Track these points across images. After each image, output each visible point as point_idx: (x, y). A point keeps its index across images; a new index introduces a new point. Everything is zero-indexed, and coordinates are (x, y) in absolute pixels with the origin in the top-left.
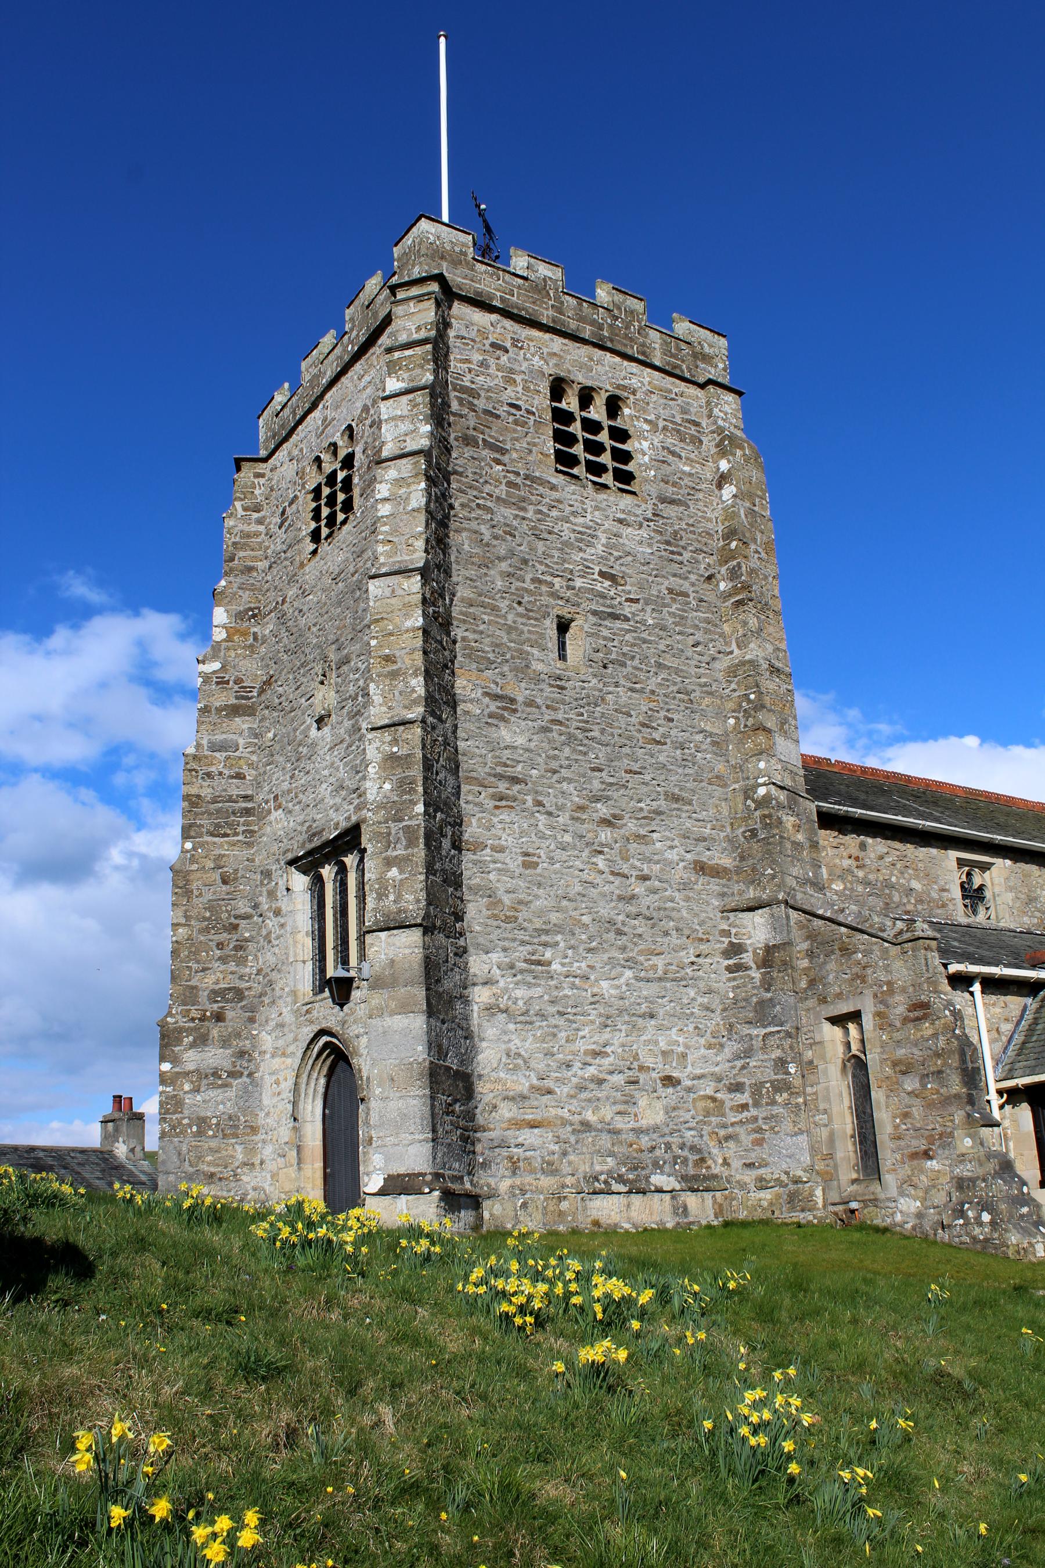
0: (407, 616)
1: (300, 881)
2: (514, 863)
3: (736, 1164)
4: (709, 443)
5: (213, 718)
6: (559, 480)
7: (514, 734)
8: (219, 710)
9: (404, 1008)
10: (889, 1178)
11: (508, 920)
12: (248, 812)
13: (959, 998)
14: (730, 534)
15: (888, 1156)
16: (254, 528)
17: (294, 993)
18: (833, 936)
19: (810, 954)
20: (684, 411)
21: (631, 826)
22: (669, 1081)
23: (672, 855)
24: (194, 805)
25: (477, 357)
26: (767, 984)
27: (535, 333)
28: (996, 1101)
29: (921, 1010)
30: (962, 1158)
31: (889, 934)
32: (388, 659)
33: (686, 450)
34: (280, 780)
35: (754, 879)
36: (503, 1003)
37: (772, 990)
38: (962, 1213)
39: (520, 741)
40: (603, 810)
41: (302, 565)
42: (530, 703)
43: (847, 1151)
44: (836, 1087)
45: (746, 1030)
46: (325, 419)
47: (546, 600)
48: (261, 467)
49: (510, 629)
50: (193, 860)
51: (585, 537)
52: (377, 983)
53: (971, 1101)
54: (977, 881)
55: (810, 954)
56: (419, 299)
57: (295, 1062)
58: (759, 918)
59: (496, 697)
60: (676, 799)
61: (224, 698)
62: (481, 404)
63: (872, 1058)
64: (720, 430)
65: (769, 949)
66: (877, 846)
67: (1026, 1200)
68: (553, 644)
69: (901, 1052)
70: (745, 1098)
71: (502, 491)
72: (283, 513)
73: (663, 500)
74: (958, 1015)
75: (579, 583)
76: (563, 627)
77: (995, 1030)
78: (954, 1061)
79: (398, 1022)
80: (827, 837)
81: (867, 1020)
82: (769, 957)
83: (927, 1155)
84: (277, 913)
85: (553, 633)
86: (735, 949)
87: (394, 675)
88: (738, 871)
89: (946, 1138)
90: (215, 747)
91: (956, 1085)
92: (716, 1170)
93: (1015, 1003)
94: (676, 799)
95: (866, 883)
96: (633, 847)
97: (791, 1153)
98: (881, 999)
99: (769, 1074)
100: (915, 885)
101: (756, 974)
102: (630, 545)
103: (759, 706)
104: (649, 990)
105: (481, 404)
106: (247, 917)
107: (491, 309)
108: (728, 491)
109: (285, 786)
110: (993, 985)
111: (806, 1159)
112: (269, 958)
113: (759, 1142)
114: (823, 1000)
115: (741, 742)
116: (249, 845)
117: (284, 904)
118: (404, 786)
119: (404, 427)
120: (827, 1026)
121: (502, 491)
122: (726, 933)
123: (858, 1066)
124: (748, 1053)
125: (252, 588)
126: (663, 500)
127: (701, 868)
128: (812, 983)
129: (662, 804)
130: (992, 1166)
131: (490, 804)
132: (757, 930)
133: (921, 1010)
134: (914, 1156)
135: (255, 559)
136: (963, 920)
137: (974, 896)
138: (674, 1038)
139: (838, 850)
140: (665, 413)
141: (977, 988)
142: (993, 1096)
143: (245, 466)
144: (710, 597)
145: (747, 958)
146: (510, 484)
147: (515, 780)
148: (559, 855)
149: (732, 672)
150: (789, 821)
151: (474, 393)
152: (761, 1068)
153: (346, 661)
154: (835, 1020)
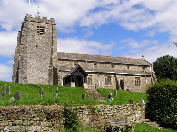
2: (31, 64)
7: (32, 55)
13: (60, 73)
40: (39, 60)
96: (41, 62)
102: (43, 39)
127: (47, 63)
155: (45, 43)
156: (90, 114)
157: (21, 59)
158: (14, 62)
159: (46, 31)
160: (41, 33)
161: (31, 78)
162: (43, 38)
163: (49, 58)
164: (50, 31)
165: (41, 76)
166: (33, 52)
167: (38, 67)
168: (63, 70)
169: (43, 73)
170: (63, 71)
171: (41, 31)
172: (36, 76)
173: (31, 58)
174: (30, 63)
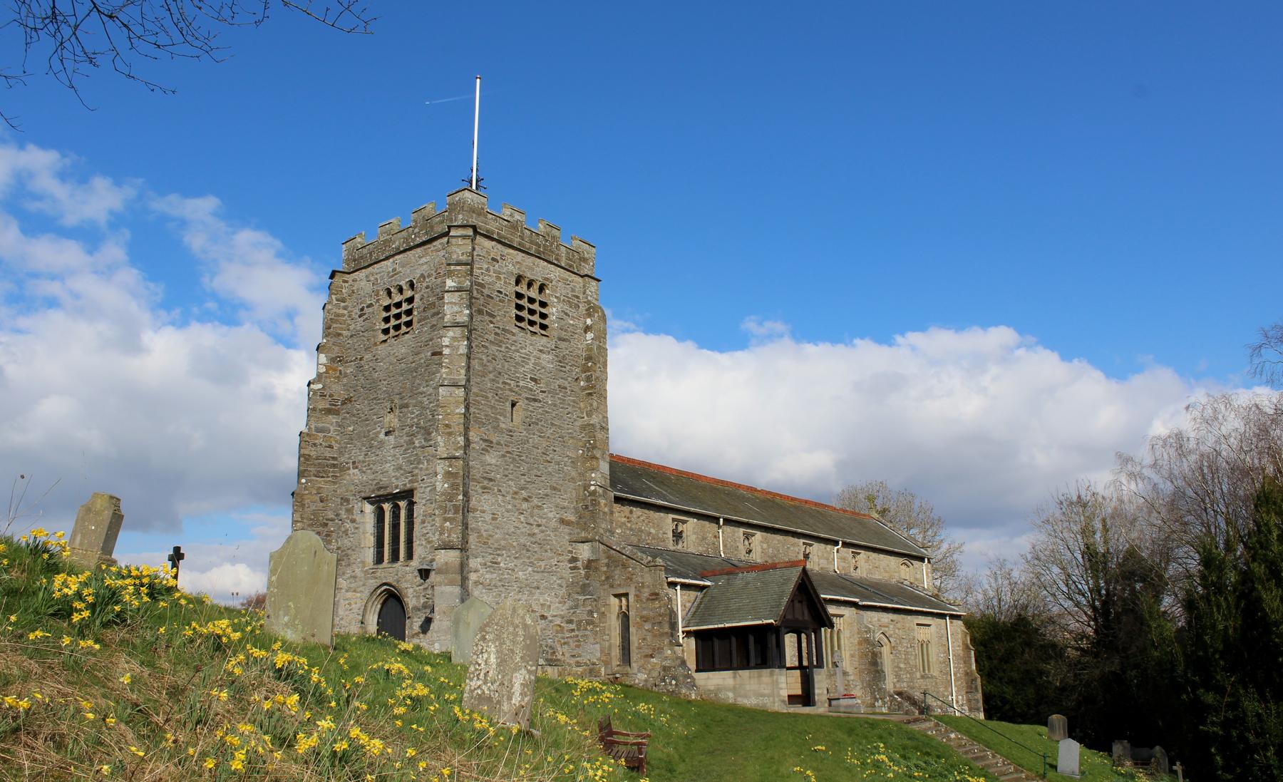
0: (457, 407)
1: (369, 508)
2: (488, 517)
3: (567, 655)
4: (583, 308)
5: (318, 414)
6: (516, 330)
7: (491, 458)
8: (321, 410)
9: (451, 583)
10: (634, 665)
11: (485, 543)
12: (334, 466)
13: (671, 591)
14: (589, 358)
15: (635, 656)
16: (341, 311)
17: (363, 562)
18: (616, 559)
19: (608, 565)
20: (573, 290)
21: (535, 501)
22: (543, 617)
23: (551, 515)
24: (307, 460)
25: (485, 266)
26: (587, 577)
27: (511, 251)
28: (681, 635)
29: (655, 596)
30: (666, 658)
31: (645, 562)
32: (447, 426)
33: (572, 312)
34: (356, 453)
35: (585, 528)
36: (481, 580)
37: (589, 580)
38: (664, 681)
39: (494, 461)
40: (524, 494)
41: (375, 344)
42: (499, 444)
43: (616, 652)
44: (614, 624)
45: (576, 596)
46: (394, 270)
47: (508, 392)
48: (347, 277)
49: (492, 407)
50: (306, 488)
51: (525, 360)
52: (439, 572)
53: (672, 635)
54: (680, 529)
55: (608, 565)
56: (464, 237)
57: (367, 593)
58: (586, 546)
59: (485, 441)
60: (555, 489)
61: (323, 405)
62: (486, 291)
63: (632, 614)
64: (589, 302)
65: (590, 561)
66: (637, 511)
67: (689, 676)
68: (509, 415)
69: (645, 613)
70: (573, 626)
71: (492, 337)
72: (362, 309)
73: (560, 339)
74: (670, 599)
75: (521, 384)
76: (513, 405)
77: (684, 606)
78: (667, 619)
79: (448, 589)
80: (617, 507)
81: (631, 598)
82: (589, 565)
83: (652, 656)
84: (353, 521)
85: (509, 409)
86: (574, 560)
87: (450, 434)
88: (578, 523)
89: (660, 650)
90: (319, 430)
91: (667, 629)
92: (559, 657)
93: (693, 594)
94: (555, 489)
95: (631, 529)
96: (536, 511)
97: (592, 652)
98: (639, 589)
99: (585, 617)
100: (653, 531)
101: (583, 572)
102: (544, 363)
103: (594, 447)
104: (537, 576)
105: (486, 291)
106: (332, 520)
107: (493, 239)
108: (590, 336)
109: (361, 458)
110: (685, 587)
111: (598, 655)
112: (346, 542)
113: (578, 646)
114: (612, 586)
115: (584, 463)
116: (335, 483)
117: (358, 518)
118: (454, 486)
119: (456, 308)
120: (612, 598)
121: (492, 337)
122: (571, 552)
123: (625, 618)
124: (576, 607)
125: (339, 345)
126: (560, 339)
127: (562, 521)
128: (607, 578)
129: (549, 491)
130: (678, 662)
131: (480, 491)
132: (585, 552)
133: (655, 596)
134: (646, 656)
135: (342, 329)
136: (672, 548)
137: (678, 536)
138: (547, 598)
139: (621, 512)
140: (564, 292)
141: (678, 588)
142: (681, 635)
143: (338, 276)
144: (576, 389)
145: (579, 564)
146: (496, 334)
147: (491, 480)
148: (506, 514)
149: (583, 428)
150: (603, 502)
151: (482, 286)
152: (582, 614)
153: (406, 406)
154: (616, 596)
159: (553, 311)
160: (532, 323)
169: (544, 584)
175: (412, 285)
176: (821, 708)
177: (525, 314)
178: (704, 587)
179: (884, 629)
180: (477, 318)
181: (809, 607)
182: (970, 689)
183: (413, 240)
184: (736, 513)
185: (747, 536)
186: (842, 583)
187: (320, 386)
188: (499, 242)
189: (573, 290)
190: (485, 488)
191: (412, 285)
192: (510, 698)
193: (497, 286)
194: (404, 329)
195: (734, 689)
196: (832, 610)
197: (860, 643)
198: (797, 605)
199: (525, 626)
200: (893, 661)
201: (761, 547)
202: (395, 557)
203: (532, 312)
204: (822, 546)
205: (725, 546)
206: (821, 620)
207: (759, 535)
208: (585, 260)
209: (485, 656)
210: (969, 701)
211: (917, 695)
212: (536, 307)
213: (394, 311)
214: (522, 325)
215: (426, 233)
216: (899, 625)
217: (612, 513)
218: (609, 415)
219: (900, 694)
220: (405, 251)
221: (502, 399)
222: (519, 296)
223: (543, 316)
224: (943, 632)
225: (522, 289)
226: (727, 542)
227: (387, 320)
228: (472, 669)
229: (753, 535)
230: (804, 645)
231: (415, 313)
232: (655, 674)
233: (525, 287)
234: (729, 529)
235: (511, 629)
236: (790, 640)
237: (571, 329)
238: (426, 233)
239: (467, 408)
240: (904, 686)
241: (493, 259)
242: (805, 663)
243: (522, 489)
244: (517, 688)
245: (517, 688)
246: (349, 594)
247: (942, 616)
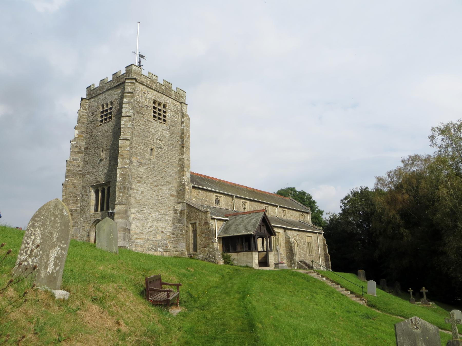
0: (126, 148)
2: (140, 192)
7: (142, 170)
8: (75, 152)
10: (198, 251)
11: (138, 203)
13: (213, 222)
15: (198, 247)
16: (85, 114)
22: (162, 232)
23: (166, 192)
25: (140, 95)
26: (181, 216)
32: (122, 155)
36: (136, 217)
39: (143, 171)
40: (155, 184)
41: (97, 126)
42: (145, 164)
46: (105, 97)
47: (149, 144)
49: (142, 150)
50: (67, 183)
51: (157, 132)
54: (218, 200)
56: (131, 83)
57: (91, 223)
58: (180, 205)
59: (139, 162)
60: (168, 182)
61: (76, 150)
62: (140, 105)
66: (202, 192)
68: (150, 153)
73: (171, 126)
80: (193, 190)
81: (197, 224)
82: (182, 212)
87: (123, 158)
90: (74, 160)
93: (222, 223)
94: (168, 182)
95: (199, 199)
96: (160, 191)
100: (207, 200)
102: (165, 134)
104: (160, 216)
105: (140, 105)
106: (79, 195)
109: (91, 171)
113: (176, 244)
114: (190, 220)
119: (127, 110)
121: (143, 123)
122: (174, 207)
124: (176, 228)
126: (171, 126)
127: (171, 195)
129: (166, 183)
132: (180, 207)
134: (203, 247)
135: (85, 121)
136: (215, 206)
137: (217, 202)
138: (164, 225)
143: (84, 100)
145: (178, 212)
146: (145, 121)
150: (187, 188)
155: (168, 146)
156: (30, 256)
157: (124, 179)
158: (66, 177)
159: (169, 115)
160: (160, 119)
161: (138, 231)
162: (445, 172)
163: (175, 181)
164: (178, 119)
165: (160, 225)
166: (145, 164)
167: (154, 202)
168: (219, 218)
169: (163, 219)
170: (218, 220)
171: (159, 113)
172: (148, 225)
173: (140, 179)
174: (138, 189)
175: (112, 103)
176: (271, 267)
177: (157, 115)
178: (226, 220)
179: (295, 238)
180: (136, 115)
181: (267, 228)
182: (326, 260)
183: (113, 85)
184: (240, 194)
185: (244, 203)
186: (279, 221)
187: (75, 142)
188: (147, 87)
189: (177, 108)
190: (139, 181)
191: (112, 103)
192: (46, 268)
193: (146, 103)
194: (108, 120)
195: (237, 260)
196: (276, 230)
197: (286, 243)
198: (262, 227)
199: (62, 216)
200: (298, 249)
201: (250, 206)
202: (102, 209)
203: (160, 114)
204: (272, 207)
205: (235, 206)
206: (271, 233)
207: (248, 202)
208: (182, 97)
209: (33, 237)
210: (326, 264)
211: (307, 262)
212: (161, 113)
213: (105, 113)
214: (156, 119)
215: (117, 82)
216: (300, 236)
217: (191, 192)
218: (191, 155)
219: (301, 262)
220: (109, 89)
221: (147, 147)
222: (154, 108)
223: (164, 116)
224: (316, 239)
225: (156, 106)
226: (238, 205)
227: (102, 117)
228: (23, 246)
229: (246, 203)
230: (265, 243)
231: (113, 113)
232: (206, 254)
233: (157, 105)
234: (237, 200)
235: (53, 218)
236: (259, 241)
237: (176, 122)
238: (117, 82)
239: (131, 148)
240: (302, 259)
241: (144, 93)
242: (265, 250)
243: (155, 182)
244: (52, 261)
245: (52, 261)
246: (84, 225)
247: (316, 233)
